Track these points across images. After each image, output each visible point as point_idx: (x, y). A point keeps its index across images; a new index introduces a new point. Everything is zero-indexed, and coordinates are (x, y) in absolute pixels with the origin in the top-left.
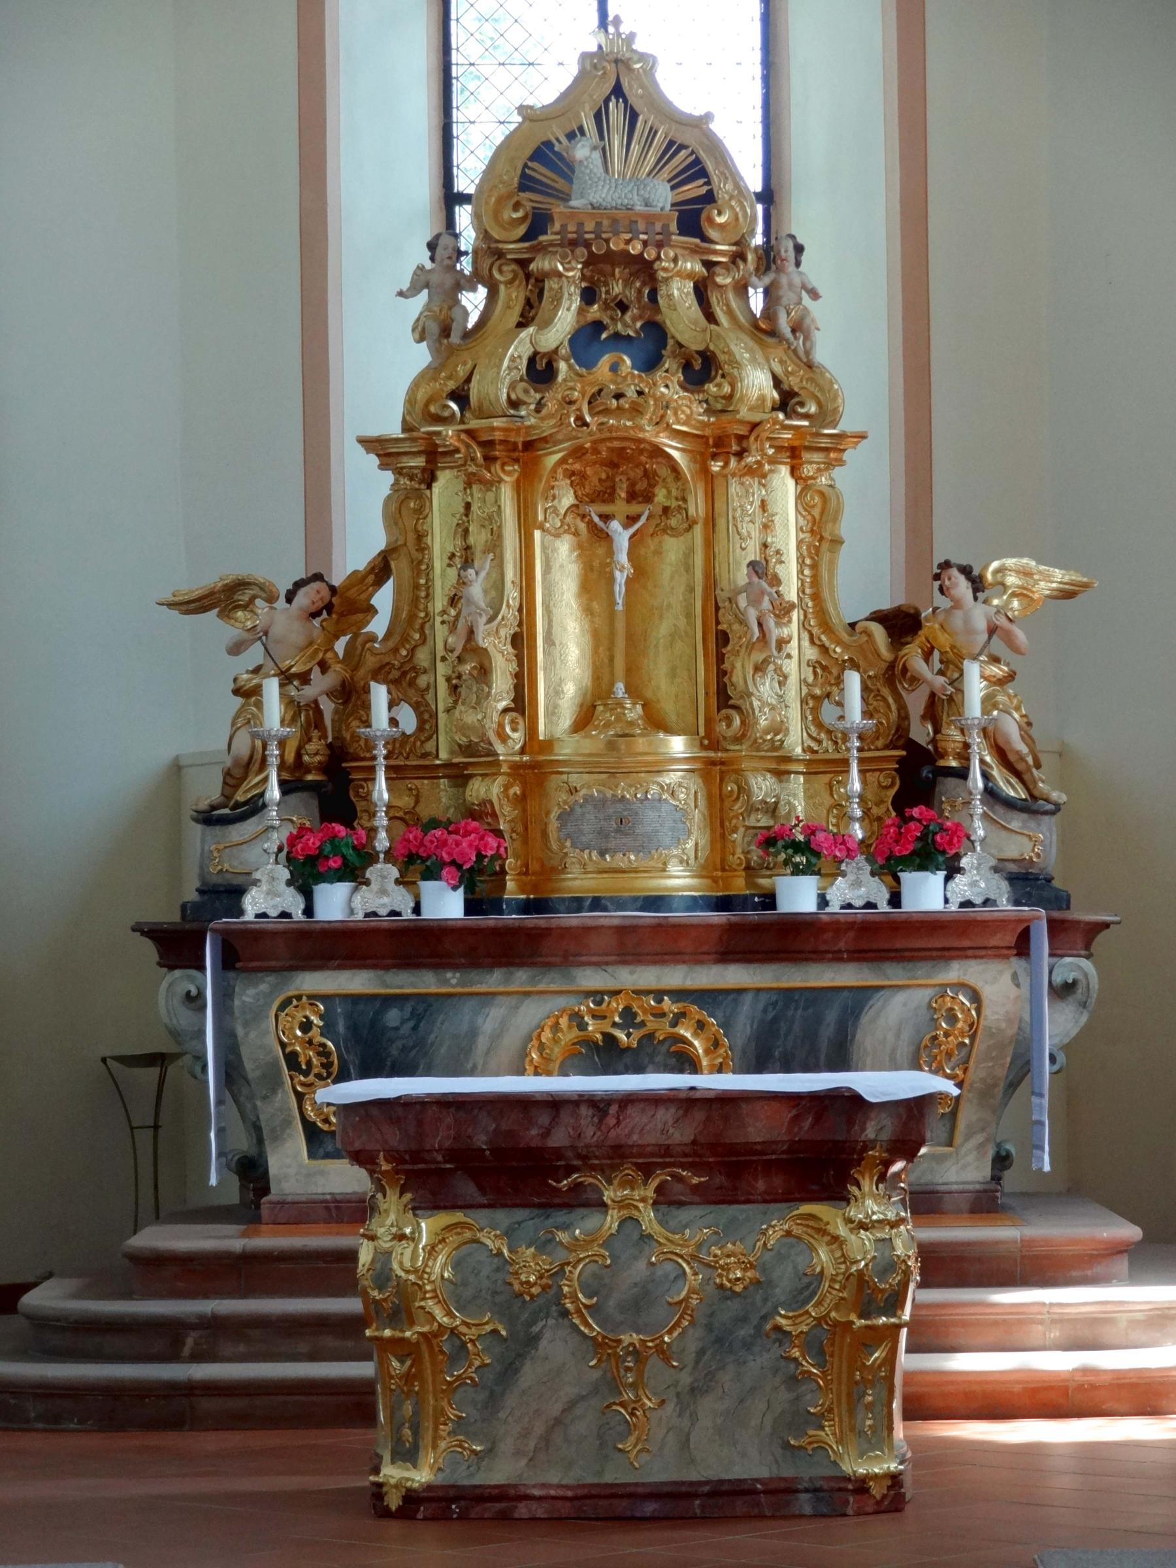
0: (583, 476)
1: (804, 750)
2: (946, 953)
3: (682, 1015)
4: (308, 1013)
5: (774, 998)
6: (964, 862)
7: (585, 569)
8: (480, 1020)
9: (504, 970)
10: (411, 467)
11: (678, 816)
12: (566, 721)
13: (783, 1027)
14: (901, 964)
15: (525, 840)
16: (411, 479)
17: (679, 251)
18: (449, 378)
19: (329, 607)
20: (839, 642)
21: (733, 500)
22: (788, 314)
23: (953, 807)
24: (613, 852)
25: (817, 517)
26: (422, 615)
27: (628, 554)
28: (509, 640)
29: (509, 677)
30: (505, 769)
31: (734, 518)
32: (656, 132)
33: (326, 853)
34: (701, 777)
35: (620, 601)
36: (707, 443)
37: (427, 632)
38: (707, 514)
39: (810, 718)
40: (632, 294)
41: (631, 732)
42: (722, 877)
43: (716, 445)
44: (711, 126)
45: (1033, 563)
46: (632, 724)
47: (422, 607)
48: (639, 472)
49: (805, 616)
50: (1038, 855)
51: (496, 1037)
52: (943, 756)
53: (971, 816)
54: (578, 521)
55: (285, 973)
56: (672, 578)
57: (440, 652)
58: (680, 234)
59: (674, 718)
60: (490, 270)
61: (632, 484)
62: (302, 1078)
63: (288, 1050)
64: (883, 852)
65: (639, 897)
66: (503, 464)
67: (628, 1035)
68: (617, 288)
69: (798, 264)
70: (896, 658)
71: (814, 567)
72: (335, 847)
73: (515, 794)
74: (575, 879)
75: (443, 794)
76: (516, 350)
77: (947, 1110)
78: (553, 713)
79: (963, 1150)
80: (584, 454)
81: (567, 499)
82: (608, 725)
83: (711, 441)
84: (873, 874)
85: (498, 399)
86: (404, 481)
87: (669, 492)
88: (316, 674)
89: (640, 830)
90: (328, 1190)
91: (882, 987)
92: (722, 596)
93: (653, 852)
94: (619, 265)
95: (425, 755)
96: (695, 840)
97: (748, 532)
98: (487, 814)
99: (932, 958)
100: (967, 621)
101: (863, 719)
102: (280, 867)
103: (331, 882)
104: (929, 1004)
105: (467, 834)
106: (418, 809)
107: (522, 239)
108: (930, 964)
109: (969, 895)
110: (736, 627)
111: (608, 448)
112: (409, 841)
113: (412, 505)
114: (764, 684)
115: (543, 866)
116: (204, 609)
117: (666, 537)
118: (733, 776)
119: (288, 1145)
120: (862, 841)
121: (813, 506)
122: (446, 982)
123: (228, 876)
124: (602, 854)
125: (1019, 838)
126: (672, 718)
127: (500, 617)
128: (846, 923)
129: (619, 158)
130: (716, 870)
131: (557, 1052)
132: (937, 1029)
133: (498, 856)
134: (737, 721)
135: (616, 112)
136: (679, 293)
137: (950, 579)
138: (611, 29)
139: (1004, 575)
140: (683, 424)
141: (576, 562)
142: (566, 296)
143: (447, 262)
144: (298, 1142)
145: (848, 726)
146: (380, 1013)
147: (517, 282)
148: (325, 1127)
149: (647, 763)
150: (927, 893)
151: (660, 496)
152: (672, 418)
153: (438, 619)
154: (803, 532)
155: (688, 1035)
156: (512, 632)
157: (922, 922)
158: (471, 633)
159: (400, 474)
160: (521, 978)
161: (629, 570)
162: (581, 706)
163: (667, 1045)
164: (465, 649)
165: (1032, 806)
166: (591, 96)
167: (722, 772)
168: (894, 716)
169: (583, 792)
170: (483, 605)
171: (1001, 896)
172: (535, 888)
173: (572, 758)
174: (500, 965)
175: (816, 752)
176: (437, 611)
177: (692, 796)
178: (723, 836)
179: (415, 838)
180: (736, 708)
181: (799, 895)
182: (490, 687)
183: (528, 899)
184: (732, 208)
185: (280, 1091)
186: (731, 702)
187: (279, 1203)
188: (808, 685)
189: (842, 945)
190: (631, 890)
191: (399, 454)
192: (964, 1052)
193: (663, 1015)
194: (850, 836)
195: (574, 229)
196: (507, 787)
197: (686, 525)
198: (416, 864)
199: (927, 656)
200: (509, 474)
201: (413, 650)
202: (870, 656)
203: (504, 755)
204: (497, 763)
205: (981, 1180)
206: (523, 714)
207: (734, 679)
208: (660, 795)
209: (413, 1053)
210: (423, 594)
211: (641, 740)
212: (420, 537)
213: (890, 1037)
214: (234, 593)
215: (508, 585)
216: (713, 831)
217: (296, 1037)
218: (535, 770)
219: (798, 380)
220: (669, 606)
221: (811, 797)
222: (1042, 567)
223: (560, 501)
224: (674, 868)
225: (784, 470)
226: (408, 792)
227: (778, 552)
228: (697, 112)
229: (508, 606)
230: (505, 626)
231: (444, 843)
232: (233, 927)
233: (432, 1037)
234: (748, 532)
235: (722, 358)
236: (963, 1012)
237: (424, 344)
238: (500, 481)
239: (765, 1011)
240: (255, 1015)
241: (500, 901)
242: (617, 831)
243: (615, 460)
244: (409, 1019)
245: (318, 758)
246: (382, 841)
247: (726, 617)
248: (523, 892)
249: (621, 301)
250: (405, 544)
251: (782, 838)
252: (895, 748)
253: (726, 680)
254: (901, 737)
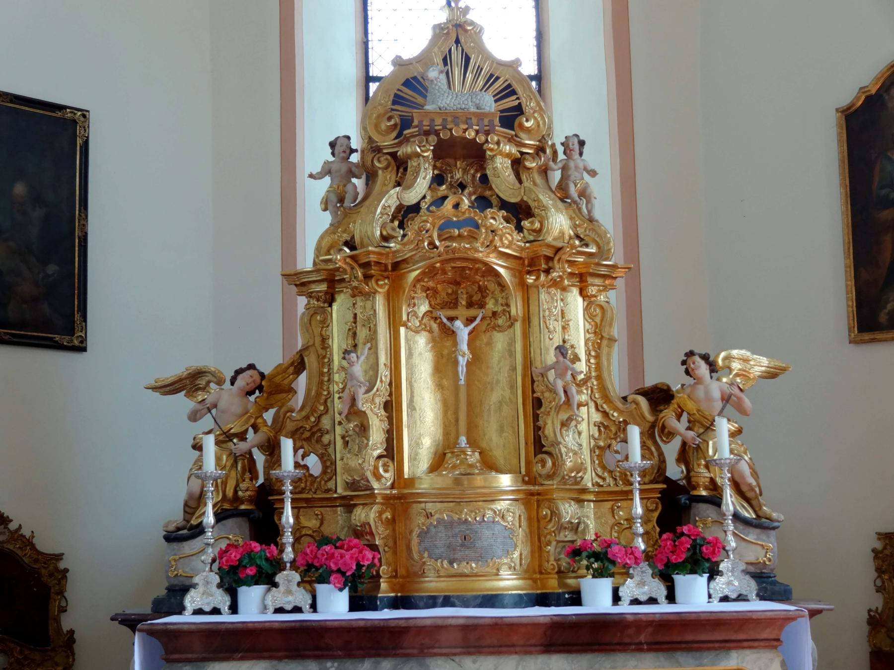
0: (435, 291)
1: (593, 485)
6: (722, 567)
9: (373, 659)
11: (507, 533)
12: (424, 464)
16: (318, 300)
17: (501, 139)
18: (344, 231)
19: (260, 388)
20: (616, 409)
22: (576, 186)
24: (460, 561)
26: (325, 393)
27: (468, 345)
28: (382, 406)
32: (482, 69)
34: (523, 504)
35: (462, 377)
36: (523, 264)
37: (329, 404)
39: (597, 462)
40: (468, 178)
41: (471, 472)
42: (540, 579)
43: (530, 265)
44: (520, 69)
45: (748, 354)
46: (471, 466)
47: (325, 388)
48: (475, 288)
49: (592, 391)
50: (770, 560)
52: (695, 488)
53: (725, 532)
54: (432, 322)
55: (199, 663)
56: (499, 361)
57: (338, 418)
58: (501, 126)
60: (372, 161)
61: (470, 297)
64: (662, 560)
65: (479, 596)
66: (377, 280)
68: (458, 175)
69: (581, 154)
70: (656, 420)
71: (597, 357)
73: (387, 518)
74: (431, 581)
76: (386, 201)
78: (415, 459)
81: (424, 308)
82: (455, 467)
83: (526, 262)
84: (653, 576)
85: (373, 235)
87: (497, 301)
89: (479, 544)
92: (536, 372)
93: (489, 560)
94: (459, 159)
95: (328, 491)
96: (519, 552)
98: (367, 533)
99: (715, 649)
101: (642, 460)
103: (249, 586)
105: (350, 548)
106: (322, 529)
107: (395, 138)
109: (726, 592)
110: (547, 394)
111: (453, 268)
112: (306, 554)
114: (568, 436)
115: (408, 571)
116: (176, 391)
117: (495, 332)
118: (547, 504)
121: (595, 316)
123: (181, 579)
124: (451, 563)
125: (754, 546)
126: (501, 462)
127: (375, 389)
128: (647, 621)
133: (372, 565)
134: (549, 463)
136: (500, 167)
137: (694, 363)
140: (507, 248)
141: (431, 351)
142: (422, 169)
143: (343, 155)
145: (633, 465)
150: (696, 595)
151: (490, 305)
152: (499, 246)
153: (337, 396)
156: (384, 400)
158: (354, 400)
159: (311, 297)
161: (469, 355)
162: (435, 454)
164: (349, 413)
165: (761, 524)
167: (538, 501)
168: (657, 459)
169: (437, 516)
170: (362, 379)
171: (751, 592)
172: (402, 587)
175: (602, 486)
177: (517, 519)
178: (540, 548)
179: (312, 551)
180: (549, 453)
181: (598, 597)
182: (368, 440)
183: (396, 596)
184: (535, 118)
186: (544, 449)
188: (595, 439)
189: (642, 638)
190: (473, 590)
191: (310, 282)
194: (636, 548)
196: (381, 513)
198: (313, 574)
200: (381, 286)
202: (638, 418)
204: (373, 496)
206: (393, 459)
207: (546, 432)
208: (494, 518)
210: (326, 379)
211: (479, 477)
212: (324, 340)
214: (197, 379)
216: (532, 545)
218: (401, 500)
220: (498, 381)
224: (505, 573)
225: (575, 291)
228: (513, 58)
229: (381, 381)
231: (332, 556)
235: (532, 204)
238: (375, 292)
241: (376, 598)
242: (462, 545)
245: (248, 493)
246: (289, 554)
247: (539, 388)
248: (393, 591)
249: (461, 183)
250: (314, 344)
251: (586, 550)
252: (657, 483)
253: (540, 433)
254: (659, 473)
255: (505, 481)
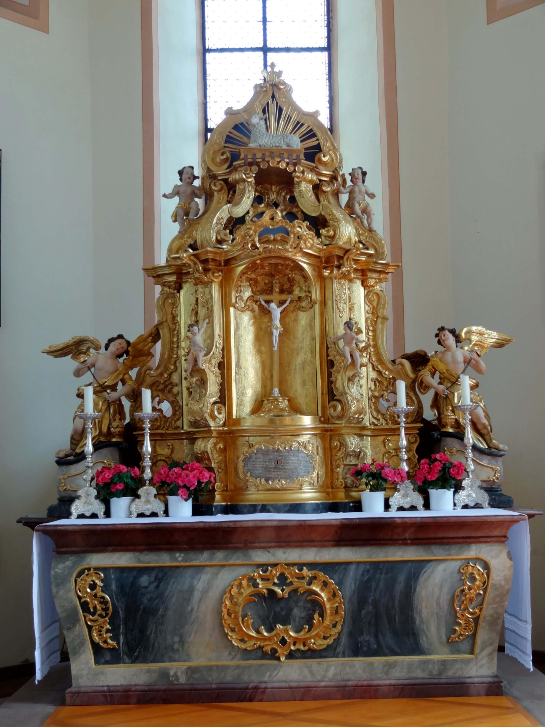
0: (256, 281)
1: (370, 424)
2: (468, 540)
3: (314, 578)
4: (94, 579)
5: (368, 567)
6: (464, 483)
7: (257, 329)
8: (195, 582)
9: (210, 551)
10: (169, 282)
11: (308, 459)
12: (247, 408)
13: (373, 585)
14: (442, 547)
15: (226, 473)
16: (169, 288)
18: (189, 237)
20: (387, 369)
21: (335, 292)
22: (360, 205)
23: (451, 453)
24: (273, 479)
25: (375, 305)
26: (175, 356)
27: (280, 321)
28: (217, 365)
29: (217, 385)
30: (214, 434)
31: (336, 300)
33: (115, 481)
35: (276, 345)
36: (321, 261)
38: (321, 299)
39: (373, 407)
40: (281, 199)
41: (282, 414)
42: (332, 492)
43: (326, 262)
45: (484, 329)
46: (282, 410)
48: (286, 279)
50: (497, 479)
51: (205, 591)
52: (444, 426)
53: (467, 458)
55: (81, 554)
56: (303, 334)
58: (305, 160)
59: (305, 407)
61: (282, 286)
62: (91, 617)
63: (83, 600)
65: (288, 504)
66: (213, 273)
67: (283, 590)
68: (273, 197)
69: (363, 182)
70: (416, 377)
71: (374, 331)
72: (120, 478)
73: (220, 448)
75: (185, 447)
76: (220, 214)
77: (470, 633)
78: (241, 405)
79: (480, 657)
80: (256, 269)
81: (247, 293)
82: (270, 411)
83: (323, 260)
86: (167, 289)
87: (301, 289)
88: (120, 385)
90: (106, 684)
91: (431, 561)
93: (295, 479)
95: (177, 428)
96: (317, 472)
97: (343, 309)
98: (205, 459)
99: (460, 543)
100: (454, 357)
102: (91, 489)
103: (119, 497)
104: (459, 570)
105: (193, 470)
106: (173, 456)
107: (227, 168)
108: (458, 546)
109: (467, 502)
110: (338, 358)
111: (270, 264)
112: (161, 474)
113: (170, 301)
114: (353, 388)
118: (337, 438)
119: (83, 656)
120: (408, 473)
121: (373, 301)
122: (176, 559)
123: (69, 492)
124: (267, 480)
126: (304, 407)
128: (411, 523)
129: (274, 127)
130: (329, 488)
131: (240, 600)
132: (464, 585)
133: (209, 482)
134: (339, 408)
135: (272, 108)
136: (304, 190)
137: (444, 336)
138: (269, 69)
139: (470, 335)
140: (309, 249)
141: (253, 325)
142: (247, 191)
143: (188, 180)
144: (89, 655)
146: (136, 578)
147: (223, 191)
148: (105, 646)
149: (292, 431)
150: (445, 504)
151: (297, 292)
152: (303, 250)
153: (183, 358)
154: (368, 313)
155: (318, 590)
156: (218, 361)
157: (455, 522)
158: (196, 361)
159: (164, 285)
160: (220, 556)
161: (280, 329)
162: (256, 401)
163: (304, 597)
165: (492, 453)
166: (260, 102)
167: (331, 435)
170: (202, 345)
171: (484, 502)
172: (231, 499)
173: (250, 428)
174: (208, 549)
175: (377, 425)
176: (182, 354)
177: (315, 448)
178: (332, 470)
179: (165, 472)
181: (374, 506)
182: (206, 391)
183: (227, 505)
185: (78, 625)
186: (335, 398)
187: (76, 693)
188: (372, 391)
189: (407, 535)
192: (480, 598)
193: (303, 578)
194: (402, 470)
195: (251, 157)
196: (215, 444)
197: (310, 305)
198: (166, 489)
199: (433, 375)
200: (216, 277)
201: (170, 375)
203: (213, 427)
204: (210, 431)
205: (491, 674)
206: (225, 405)
207: (337, 385)
208: (298, 448)
209: (156, 601)
210: (175, 346)
211: (287, 418)
212: (174, 317)
213: (437, 590)
214: (80, 346)
215: (216, 336)
217: (87, 592)
218: (231, 435)
219: (365, 238)
221: (374, 448)
222: (488, 331)
223: (244, 293)
225: (359, 282)
226: (167, 447)
227: (356, 323)
229: (216, 347)
230: (215, 358)
232: (49, 528)
233: (167, 592)
234: (343, 309)
235: (328, 217)
236: (479, 575)
237: (177, 223)
238: (212, 281)
239: (363, 575)
240: (62, 581)
242: (275, 468)
243: (273, 273)
244: (154, 582)
245: (118, 429)
246: (148, 474)
247: (332, 352)
249: (275, 202)
250: (167, 321)
251: (365, 471)
252: (416, 423)
253: (333, 386)
254: (417, 416)
255: (307, 421)
